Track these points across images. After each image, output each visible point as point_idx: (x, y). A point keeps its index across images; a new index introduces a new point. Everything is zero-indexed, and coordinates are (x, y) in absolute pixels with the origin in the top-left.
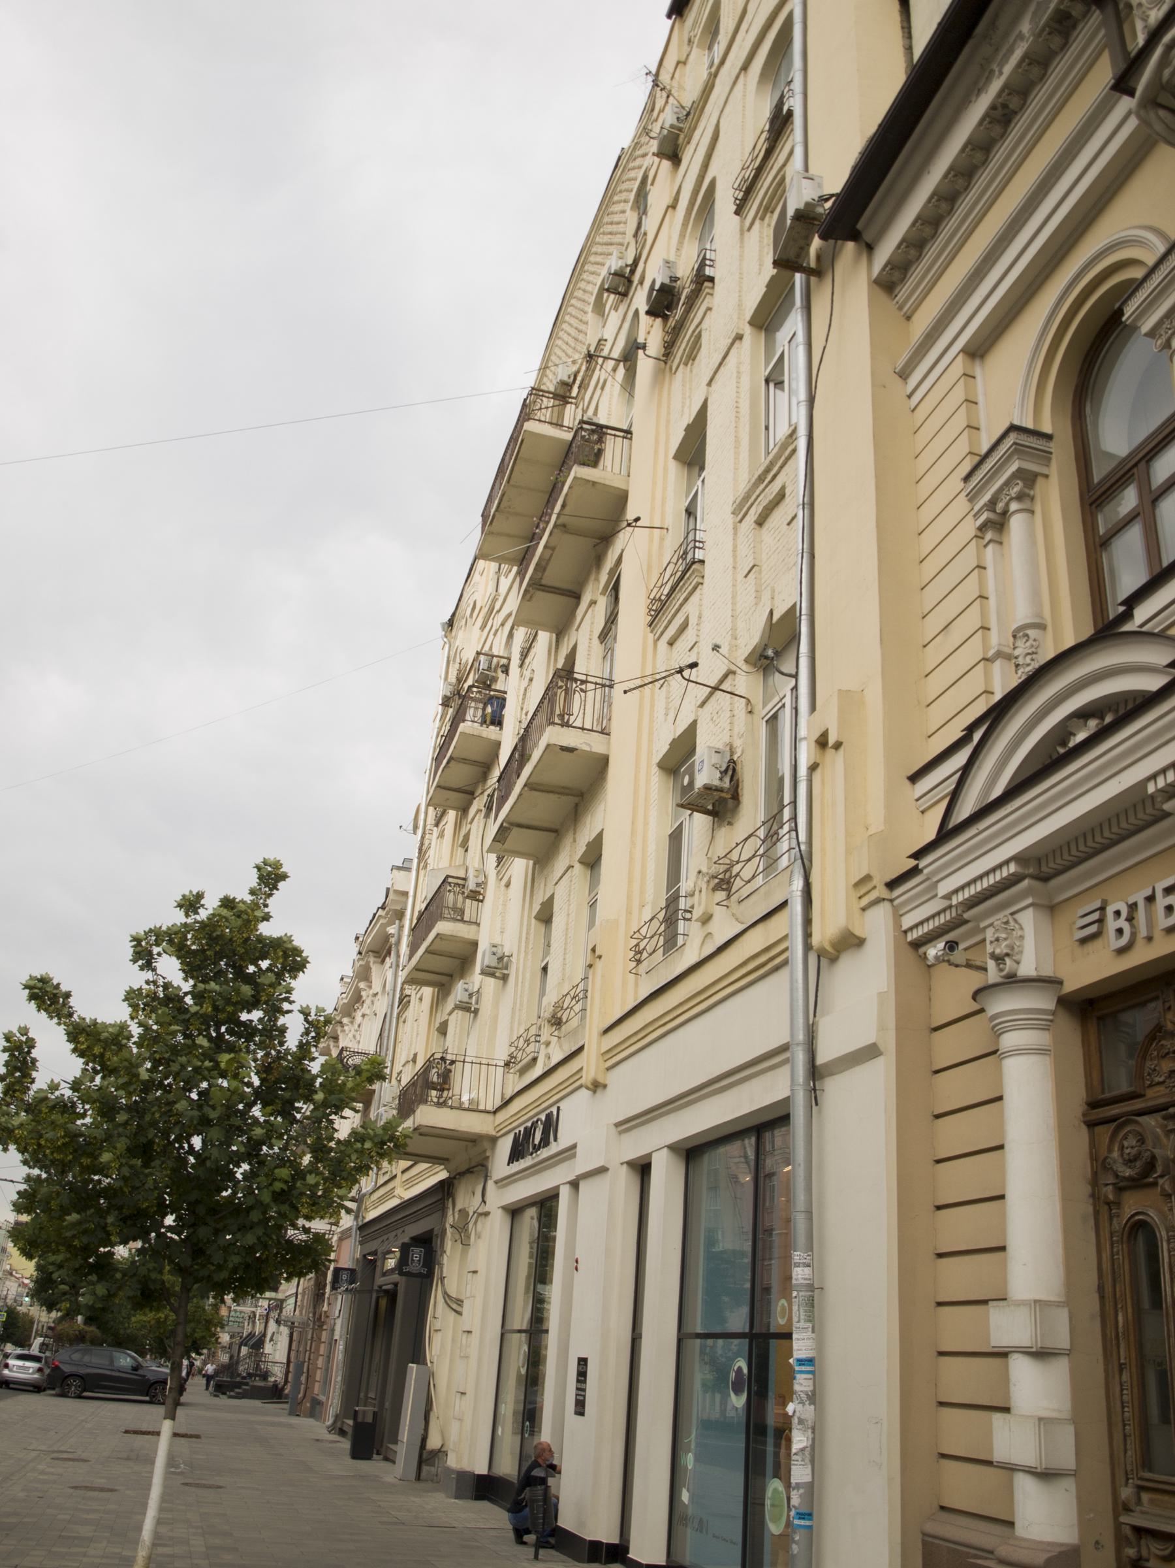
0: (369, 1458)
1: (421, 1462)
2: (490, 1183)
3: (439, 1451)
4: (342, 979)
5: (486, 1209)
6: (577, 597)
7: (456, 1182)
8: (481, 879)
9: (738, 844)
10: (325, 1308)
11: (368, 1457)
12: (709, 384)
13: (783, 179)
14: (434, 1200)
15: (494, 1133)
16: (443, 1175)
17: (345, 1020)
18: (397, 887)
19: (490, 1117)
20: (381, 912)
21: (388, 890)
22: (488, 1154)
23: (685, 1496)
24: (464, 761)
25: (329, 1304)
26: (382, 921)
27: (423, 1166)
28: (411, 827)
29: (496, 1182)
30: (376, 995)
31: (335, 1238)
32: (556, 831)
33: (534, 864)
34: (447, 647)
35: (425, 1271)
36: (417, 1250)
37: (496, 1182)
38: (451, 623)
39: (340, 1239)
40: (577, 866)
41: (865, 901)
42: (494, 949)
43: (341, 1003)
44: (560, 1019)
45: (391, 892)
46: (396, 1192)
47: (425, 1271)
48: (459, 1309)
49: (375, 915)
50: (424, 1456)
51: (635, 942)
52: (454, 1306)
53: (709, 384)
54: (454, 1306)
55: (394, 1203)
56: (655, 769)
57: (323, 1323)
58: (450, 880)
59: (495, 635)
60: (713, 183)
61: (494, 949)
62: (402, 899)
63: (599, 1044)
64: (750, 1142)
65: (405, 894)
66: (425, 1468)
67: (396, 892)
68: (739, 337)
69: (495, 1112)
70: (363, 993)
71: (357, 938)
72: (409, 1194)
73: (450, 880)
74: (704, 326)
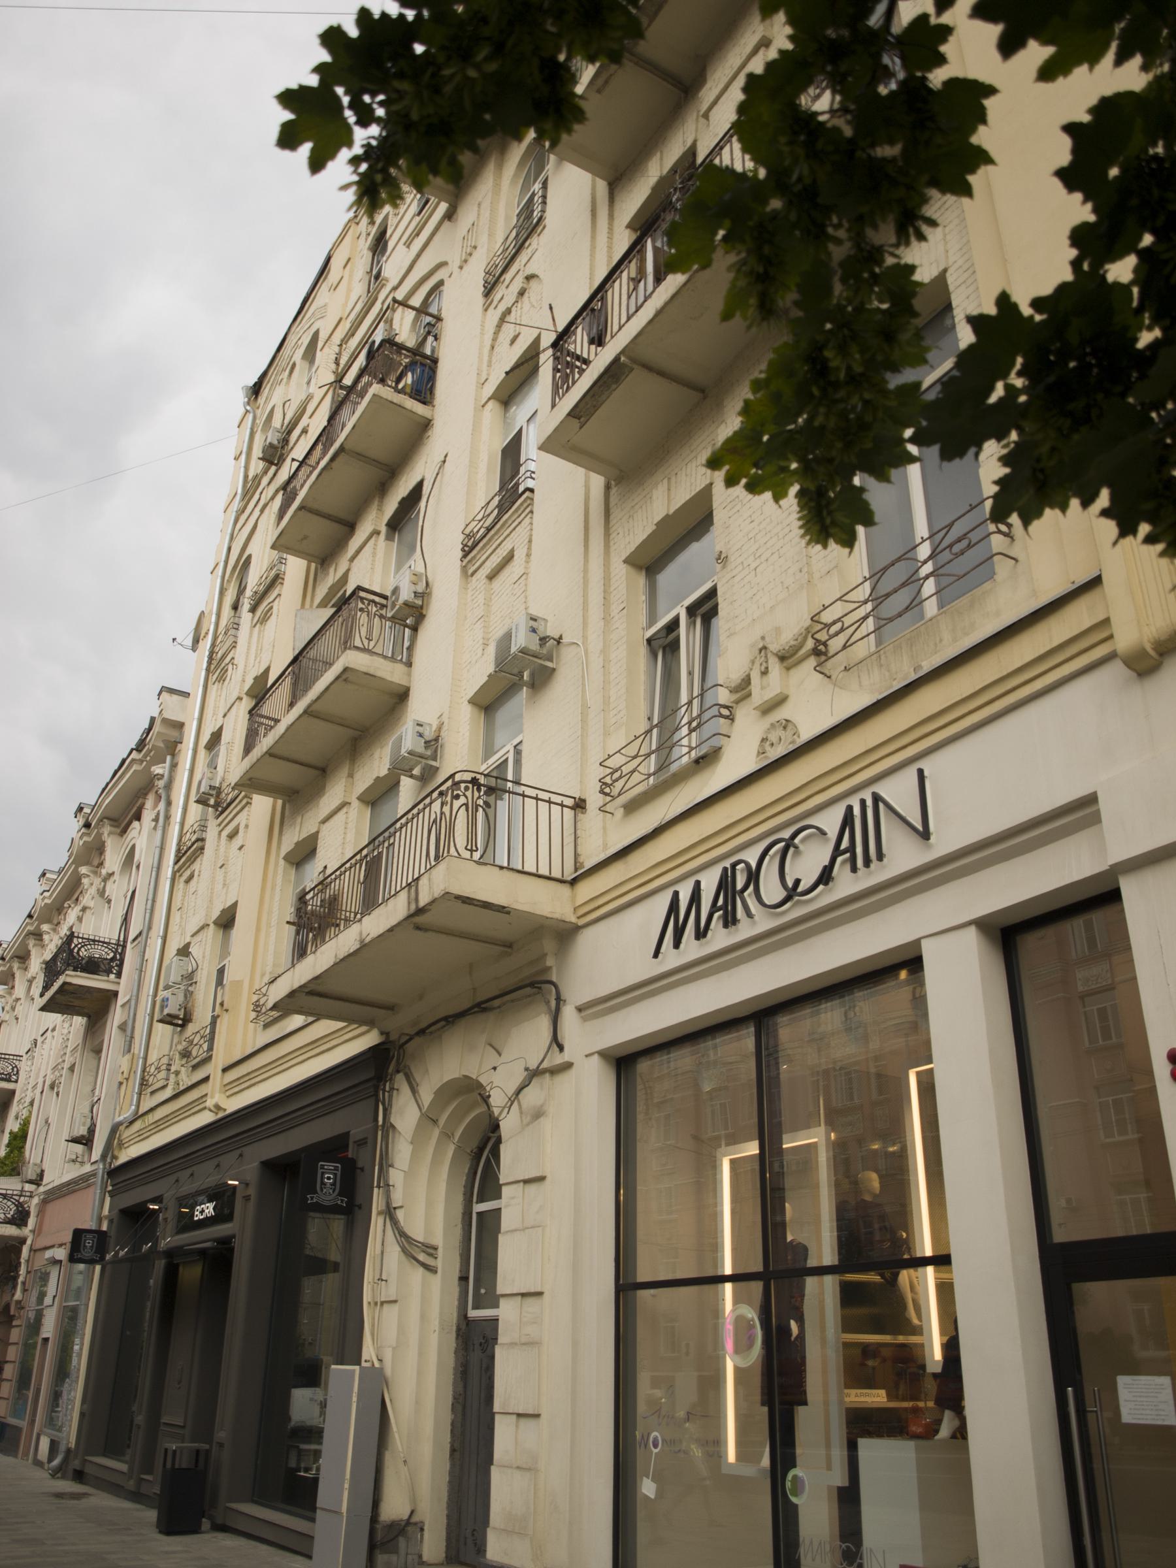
0: (195, 1530)
1: (372, 1547)
2: (569, 1014)
3: (408, 1522)
4: (44, 874)
5: (566, 1057)
6: (350, 527)
7: (410, 1047)
8: (421, 588)
9: (636, 738)
10: (18, 1295)
11: (193, 1529)
12: (225, 716)
13: (271, 608)
14: (363, 1078)
15: (573, 919)
16: (362, 1041)
17: (45, 927)
18: (166, 715)
19: (565, 890)
20: (134, 755)
21: (153, 720)
22: (550, 962)
23: (648, 1488)
24: (360, 456)
25: (25, 1290)
26: (135, 767)
27: (326, 1026)
28: (189, 642)
29: (580, 1009)
30: (18, 1000)
31: (35, 1201)
32: (702, 391)
33: (608, 487)
34: (250, 417)
35: (342, 1202)
36: (329, 1166)
37: (580, 1009)
38: (256, 390)
39: (45, 1202)
40: (356, 804)
41: (228, 1093)
42: (534, 624)
43: (41, 904)
44: (190, 1053)
45: (158, 723)
46: (210, 1103)
47: (342, 1202)
48: (430, 1261)
49: (124, 761)
50: (379, 1536)
51: (255, 998)
52: (422, 1257)
53: (225, 716)
54: (422, 1257)
55: (206, 1118)
56: (282, 862)
57: (12, 1318)
58: (362, 594)
59: (262, 511)
60: (250, 556)
61: (534, 624)
62: (173, 734)
63: (222, 1078)
64: (746, 1040)
65: (180, 726)
66: (381, 1558)
67: (167, 722)
68: (240, 699)
69: (573, 882)
70: (85, 881)
71: (80, 809)
72: (233, 1105)
73: (362, 594)
74: (275, 604)
